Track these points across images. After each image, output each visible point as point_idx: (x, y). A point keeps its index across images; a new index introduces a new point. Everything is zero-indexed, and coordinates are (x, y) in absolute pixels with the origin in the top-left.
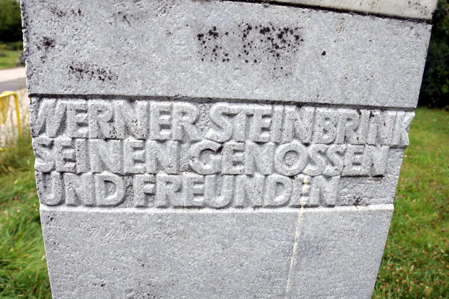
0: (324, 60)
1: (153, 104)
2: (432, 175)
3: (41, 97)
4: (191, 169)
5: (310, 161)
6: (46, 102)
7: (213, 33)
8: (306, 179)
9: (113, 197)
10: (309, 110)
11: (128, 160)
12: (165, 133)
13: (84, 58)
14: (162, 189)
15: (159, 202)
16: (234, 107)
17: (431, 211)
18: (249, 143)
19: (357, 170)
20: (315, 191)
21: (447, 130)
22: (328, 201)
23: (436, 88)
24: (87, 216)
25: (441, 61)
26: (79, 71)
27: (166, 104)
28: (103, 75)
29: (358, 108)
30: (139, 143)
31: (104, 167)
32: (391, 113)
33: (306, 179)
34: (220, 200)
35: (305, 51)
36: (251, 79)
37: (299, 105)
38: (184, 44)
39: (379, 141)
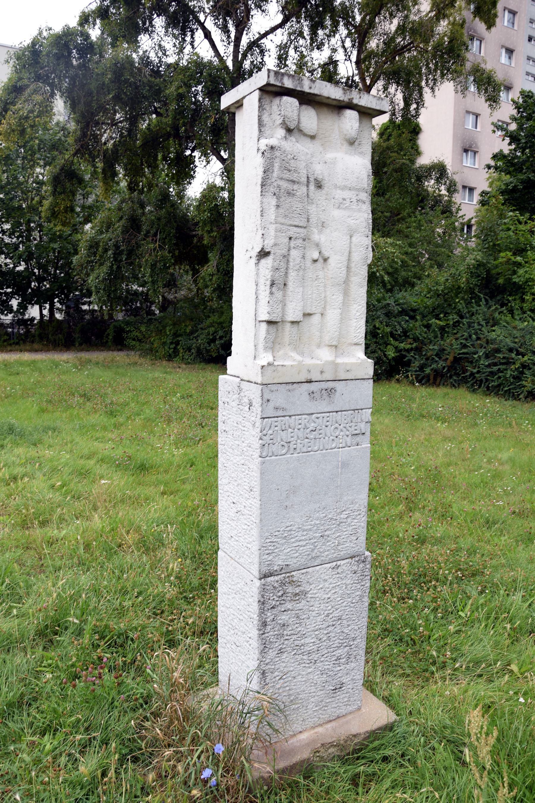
0: (343, 396)
1: (297, 417)
2: (392, 468)
3: (264, 418)
4: (307, 438)
5: (342, 431)
6: (266, 420)
7: (313, 393)
8: (341, 437)
9: (284, 451)
10: (340, 413)
11: (289, 437)
12: (300, 426)
13: (278, 405)
14: (299, 446)
15: (298, 451)
16: (319, 415)
17: (397, 506)
18: (324, 427)
19: (356, 432)
20: (344, 441)
21: (401, 411)
22: (349, 445)
23: (380, 352)
24: (276, 460)
25: (379, 313)
26: (277, 408)
27: (300, 417)
28: (284, 409)
29: (354, 410)
30: (292, 431)
31: (282, 440)
32: (364, 410)
33: (341, 437)
34: (316, 448)
35: (337, 394)
36: (323, 406)
37: (337, 412)
38: (305, 397)
39: (362, 421)
